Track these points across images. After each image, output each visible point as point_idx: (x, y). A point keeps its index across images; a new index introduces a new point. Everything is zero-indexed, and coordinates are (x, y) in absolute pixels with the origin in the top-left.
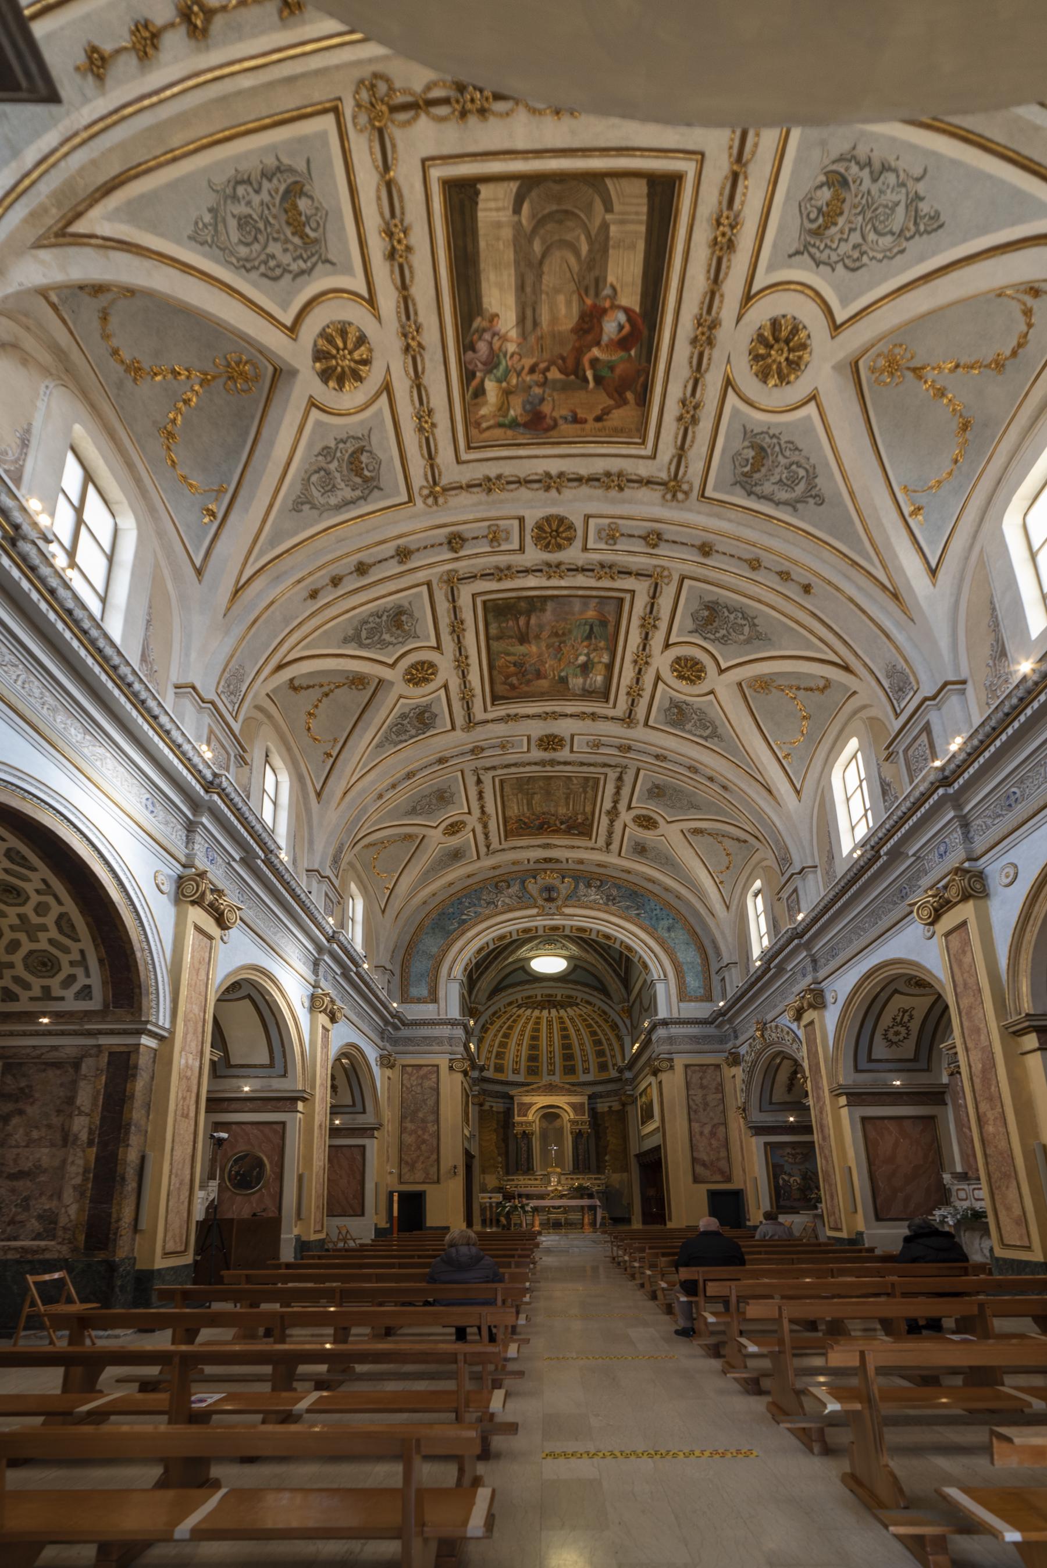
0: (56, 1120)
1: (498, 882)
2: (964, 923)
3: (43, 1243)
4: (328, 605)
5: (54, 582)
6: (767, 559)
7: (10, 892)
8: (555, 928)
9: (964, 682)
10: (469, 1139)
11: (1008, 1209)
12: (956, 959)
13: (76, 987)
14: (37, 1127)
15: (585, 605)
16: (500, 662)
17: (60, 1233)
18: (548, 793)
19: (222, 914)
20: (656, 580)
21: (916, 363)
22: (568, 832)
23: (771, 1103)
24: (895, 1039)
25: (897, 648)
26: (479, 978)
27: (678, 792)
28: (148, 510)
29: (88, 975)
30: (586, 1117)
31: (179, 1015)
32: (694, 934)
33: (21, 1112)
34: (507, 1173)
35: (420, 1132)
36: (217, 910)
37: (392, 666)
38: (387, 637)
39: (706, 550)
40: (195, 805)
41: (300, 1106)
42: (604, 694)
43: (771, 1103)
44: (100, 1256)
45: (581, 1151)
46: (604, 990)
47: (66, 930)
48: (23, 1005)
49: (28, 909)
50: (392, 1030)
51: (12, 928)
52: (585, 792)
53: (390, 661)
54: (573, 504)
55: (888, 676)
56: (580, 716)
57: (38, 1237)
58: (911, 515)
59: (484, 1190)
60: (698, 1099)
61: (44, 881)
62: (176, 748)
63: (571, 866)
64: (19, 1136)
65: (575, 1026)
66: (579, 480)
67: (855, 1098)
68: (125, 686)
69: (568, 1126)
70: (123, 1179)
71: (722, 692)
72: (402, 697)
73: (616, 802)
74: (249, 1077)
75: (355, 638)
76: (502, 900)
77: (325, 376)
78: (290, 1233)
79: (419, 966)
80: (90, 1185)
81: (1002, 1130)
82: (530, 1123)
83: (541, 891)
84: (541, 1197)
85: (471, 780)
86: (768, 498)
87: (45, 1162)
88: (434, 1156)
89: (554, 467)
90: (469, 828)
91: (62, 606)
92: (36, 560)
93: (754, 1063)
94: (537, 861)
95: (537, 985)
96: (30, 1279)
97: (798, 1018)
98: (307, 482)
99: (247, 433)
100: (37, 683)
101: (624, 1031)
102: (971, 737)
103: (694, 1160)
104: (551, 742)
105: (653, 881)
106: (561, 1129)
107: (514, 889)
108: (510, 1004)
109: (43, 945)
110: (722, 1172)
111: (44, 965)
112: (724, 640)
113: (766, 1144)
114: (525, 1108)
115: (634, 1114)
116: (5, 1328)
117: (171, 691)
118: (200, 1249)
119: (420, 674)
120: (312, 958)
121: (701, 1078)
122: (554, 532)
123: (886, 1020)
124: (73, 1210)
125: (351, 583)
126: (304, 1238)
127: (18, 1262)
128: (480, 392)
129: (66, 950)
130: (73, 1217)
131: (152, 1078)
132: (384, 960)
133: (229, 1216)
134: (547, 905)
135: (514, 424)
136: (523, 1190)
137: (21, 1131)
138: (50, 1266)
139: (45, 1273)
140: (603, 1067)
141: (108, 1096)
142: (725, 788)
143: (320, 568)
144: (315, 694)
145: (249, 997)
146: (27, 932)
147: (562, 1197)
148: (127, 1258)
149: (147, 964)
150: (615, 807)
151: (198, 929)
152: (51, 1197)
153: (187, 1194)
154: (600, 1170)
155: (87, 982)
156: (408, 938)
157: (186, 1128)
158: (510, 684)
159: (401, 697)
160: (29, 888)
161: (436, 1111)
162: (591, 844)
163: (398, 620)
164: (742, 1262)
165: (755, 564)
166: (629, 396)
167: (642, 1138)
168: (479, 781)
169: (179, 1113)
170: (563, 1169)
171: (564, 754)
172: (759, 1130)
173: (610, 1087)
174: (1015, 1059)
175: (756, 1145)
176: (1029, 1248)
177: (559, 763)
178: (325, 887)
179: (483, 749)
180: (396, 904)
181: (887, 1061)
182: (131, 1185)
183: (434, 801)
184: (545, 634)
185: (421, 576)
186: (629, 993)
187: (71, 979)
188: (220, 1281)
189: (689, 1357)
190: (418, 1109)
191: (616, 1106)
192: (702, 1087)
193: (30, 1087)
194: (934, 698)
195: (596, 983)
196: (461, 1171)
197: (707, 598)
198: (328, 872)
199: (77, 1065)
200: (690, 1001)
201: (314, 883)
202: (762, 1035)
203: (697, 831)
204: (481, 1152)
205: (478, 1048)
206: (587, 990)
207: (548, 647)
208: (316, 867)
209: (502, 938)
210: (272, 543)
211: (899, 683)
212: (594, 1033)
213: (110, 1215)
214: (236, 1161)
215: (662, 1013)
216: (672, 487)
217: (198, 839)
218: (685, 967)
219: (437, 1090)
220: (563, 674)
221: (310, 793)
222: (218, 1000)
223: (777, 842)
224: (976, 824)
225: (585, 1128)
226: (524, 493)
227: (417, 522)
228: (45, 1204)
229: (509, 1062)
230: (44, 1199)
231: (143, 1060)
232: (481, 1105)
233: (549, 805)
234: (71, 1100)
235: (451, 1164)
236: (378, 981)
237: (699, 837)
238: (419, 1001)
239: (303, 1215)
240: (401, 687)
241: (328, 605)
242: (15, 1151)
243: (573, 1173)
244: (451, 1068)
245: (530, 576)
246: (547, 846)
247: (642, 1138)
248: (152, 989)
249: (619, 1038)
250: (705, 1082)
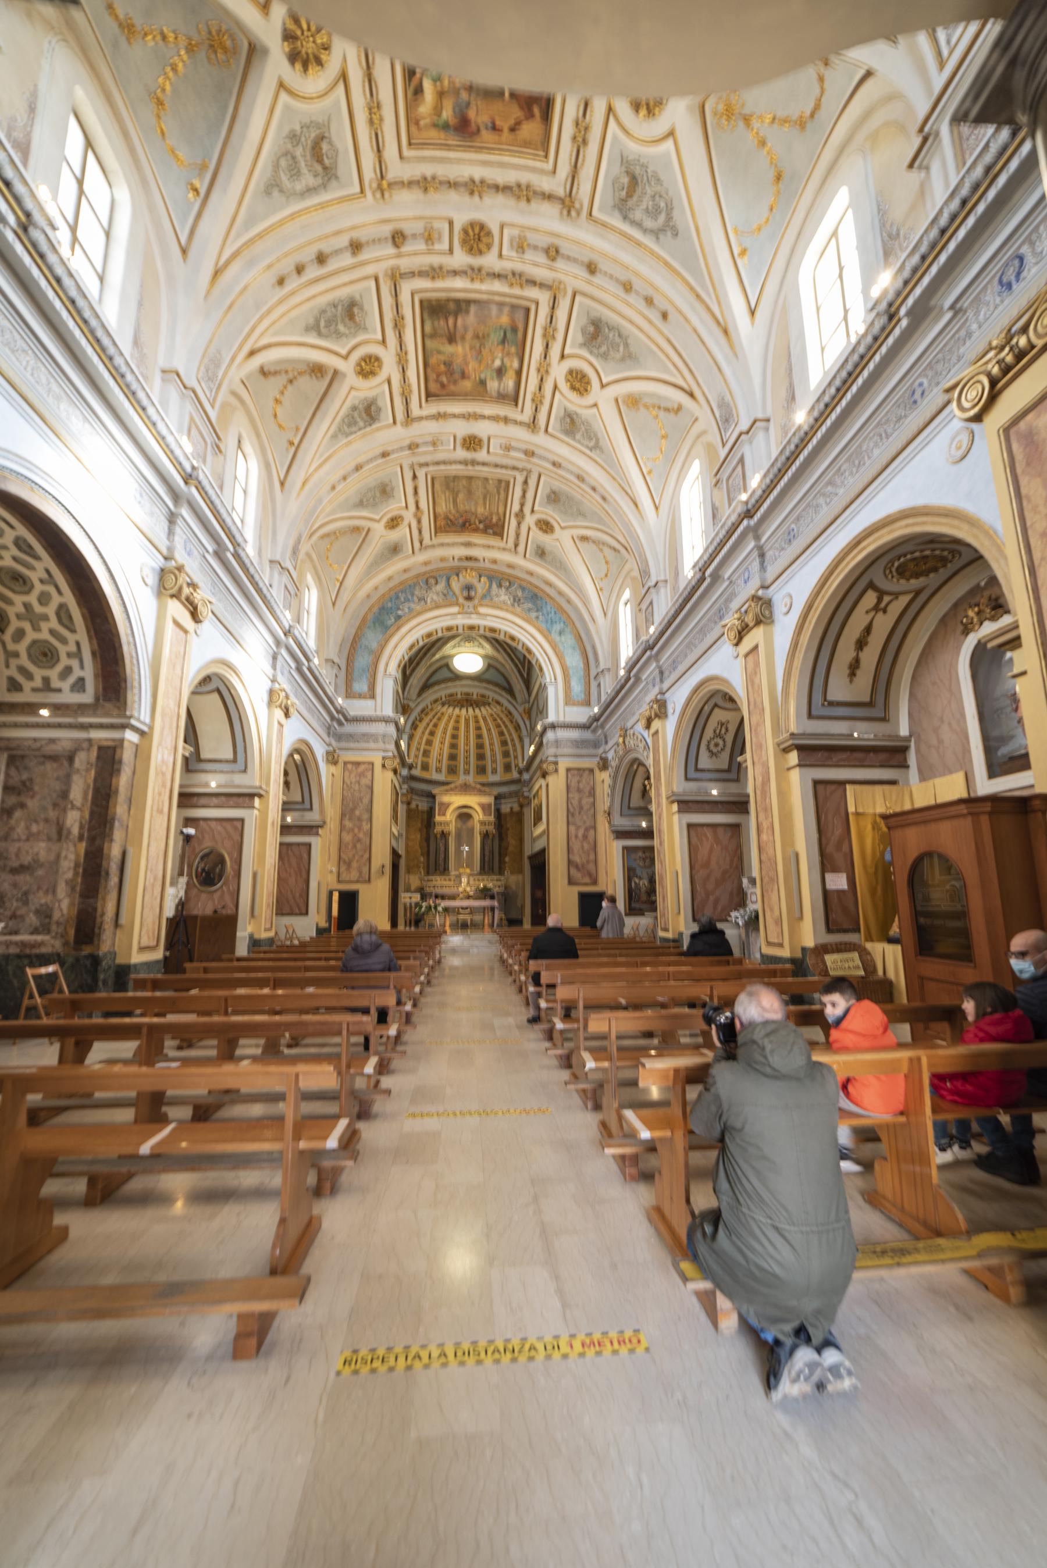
0: (52, 814)
1: (429, 579)
2: (756, 647)
3: (39, 938)
4: (293, 293)
5: (59, 271)
6: (637, 284)
7: (17, 580)
8: (472, 628)
9: (768, 420)
10: (397, 839)
11: (772, 910)
12: (751, 677)
13: (72, 679)
14: (36, 821)
15: (501, 311)
16: (433, 360)
17: (54, 927)
18: (470, 493)
19: (195, 608)
20: (554, 290)
21: (747, 111)
22: (485, 532)
23: (629, 807)
24: (715, 750)
25: (725, 381)
27: (570, 499)
28: (141, 183)
29: (82, 667)
30: (492, 818)
31: (157, 707)
32: (579, 639)
33: (22, 806)
34: (428, 873)
35: (356, 830)
36: (191, 603)
37: (346, 357)
38: (341, 328)
39: (592, 268)
40: (176, 496)
41: (257, 800)
42: (514, 399)
43: (629, 807)
44: (87, 950)
45: (487, 853)
46: (510, 691)
47: (65, 620)
48: (25, 696)
49: (32, 599)
50: (337, 723)
51: (19, 617)
52: (499, 493)
53: (344, 351)
54: (494, 212)
55: (720, 407)
56: (495, 419)
57: (35, 931)
58: (739, 255)
59: (408, 890)
60: (575, 802)
61: (48, 571)
62: (161, 439)
63: (488, 565)
64: (20, 830)
65: (487, 725)
66: (497, 188)
67: (685, 805)
68: (118, 376)
69: (477, 828)
70: (107, 874)
71: (601, 406)
72: (354, 389)
73: (522, 505)
74: (215, 772)
75: (315, 328)
76: (432, 596)
77: (293, 57)
78: (245, 930)
79: (362, 661)
80: (79, 880)
81: (771, 838)
82: (447, 824)
83: (462, 590)
84: (453, 897)
85: (408, 475)
86: (638, 225)
87: (43, 856)
88: (367, 856)
89: (478, 173)
90: (406, 522)
91: (66, 294)
92: (44, 247)
93: (618, 768)
94: (460, 559)
95: (458, 683)
96: (30, 972)
97: (648, 727)
98: (276, 166)
99: (226, 107)
100: (43, 369)
101: (524, 732)
102: (765, 476)
104: (472, 443)
105: (549, 584)
106: (471, 831)
107: (441, 586)
108: (436, 701)
109: (45, 635)
110: (590, 875)
111: (45, 655)
112: (605, 356)
113: (624, 848)
114: (445, 806)
115: (529, 815)
116: (12, 1012)
117: (158, 376)
118: (170, 945)
119: (368, 367)
120: (271, 652)
122: (476, 237)
123: (709, 733)
124: (65, 904)
125: (313, 272)
126: (256, 936)
127: (19, 956)
128: (419, 91)
129: (64, 641)
130: (65, 911)
131: (134, 773)
132: (333, 654)
133: (195, 912)
134: (467, 603)
135: (445, 127)
136: (440, 891)
137: (22, 824)
138: (45, 960)
139: (41, 965)
140: (507, 768)
141: (97, 791)
142: (604, 499)
143: (286, 255)
144: (282, 380)
145: (218, 691)
146: (31, 622)
147: (469, 897)
148: (110, 952)
149: (132, 657)
150: (521, 510)
151: (176, 623)
152: (47, 892)
153: (160, 889)
154: (501, 872)
155: (82, 674)
156: (353, 631)
157: (161, 822)
158: (442, 382)
159: (352, 388)
160: (34, 576)
161: (370, 811)
162: (502, 544)
163: (350, 311)
164: (576, 956)
165: (628, 287)
166: (536, 111)
167: (534, 840)
168: (415, 477)
169: (155, 808)
170: (472, 870)
171: (482, 455)
172: (620, 834)
173: (513, 788)
174: (783, 771)
175: (616, 848)
176: (781, 945)
177: (478, 463)
178: (285, 579)
179: (417, 446)
180: (345, 597)
181: (709, 771)
182: (114, 880)
183: (378, 494)
184: (469, 335)
185: (370, 270)
186: (530, 694)
187: (68, 670)
188: (184, 971)
189: (533, 1040)
190: (355, 809)
191: (516, 808)
192: (579, 790)
193: (31, 780)
194: (748, 432)
195: (505, 684)
196: (388, 870)
197: (593, 314)
198: (288, 564)
199: (71, 759)
200: (574, 704)
201: (276, 575)
202: (624, 742)
203: (584, 539)
204: (407, 852)
205: (409, 746)
206: (497, 689)
207: (471, 348)
208: (278, 558)
209: (429, 635)
210: (248, 225)
211: (726, 417)
212: (501, 734)
213: (95, 909)
214: (202, 858)
215: (552, 718)
216: (567, 204)
217: (178, 530)
218: (571, 672)
219: (371, 788)
220: (483, 376)
221: (279, 480)
222: (194, 693)
223: (640, 556)
224: (769, 554)
225: (491, 829)
226: (453, 196)
227: (367, 216)
228: (40, 899)
229: (433, 762)
230: (41, 894)
231: (127, 755)
232: (409, 803)
233: (471, 506)
234: (65, 794)
235: (380, 863)
236: (327, 675)
237: (585, 544)
238: (361, 696)
239: (256, 913)
240: (352, 379)
241: (293, 293)
242: (17, 845)
243: (480, 874)
244: (384, 766)
245: (458, 278)
246: (468, 545)
247: (534, 840)
248: (136, 684)
249: (521, 739)
250: (581, 786)
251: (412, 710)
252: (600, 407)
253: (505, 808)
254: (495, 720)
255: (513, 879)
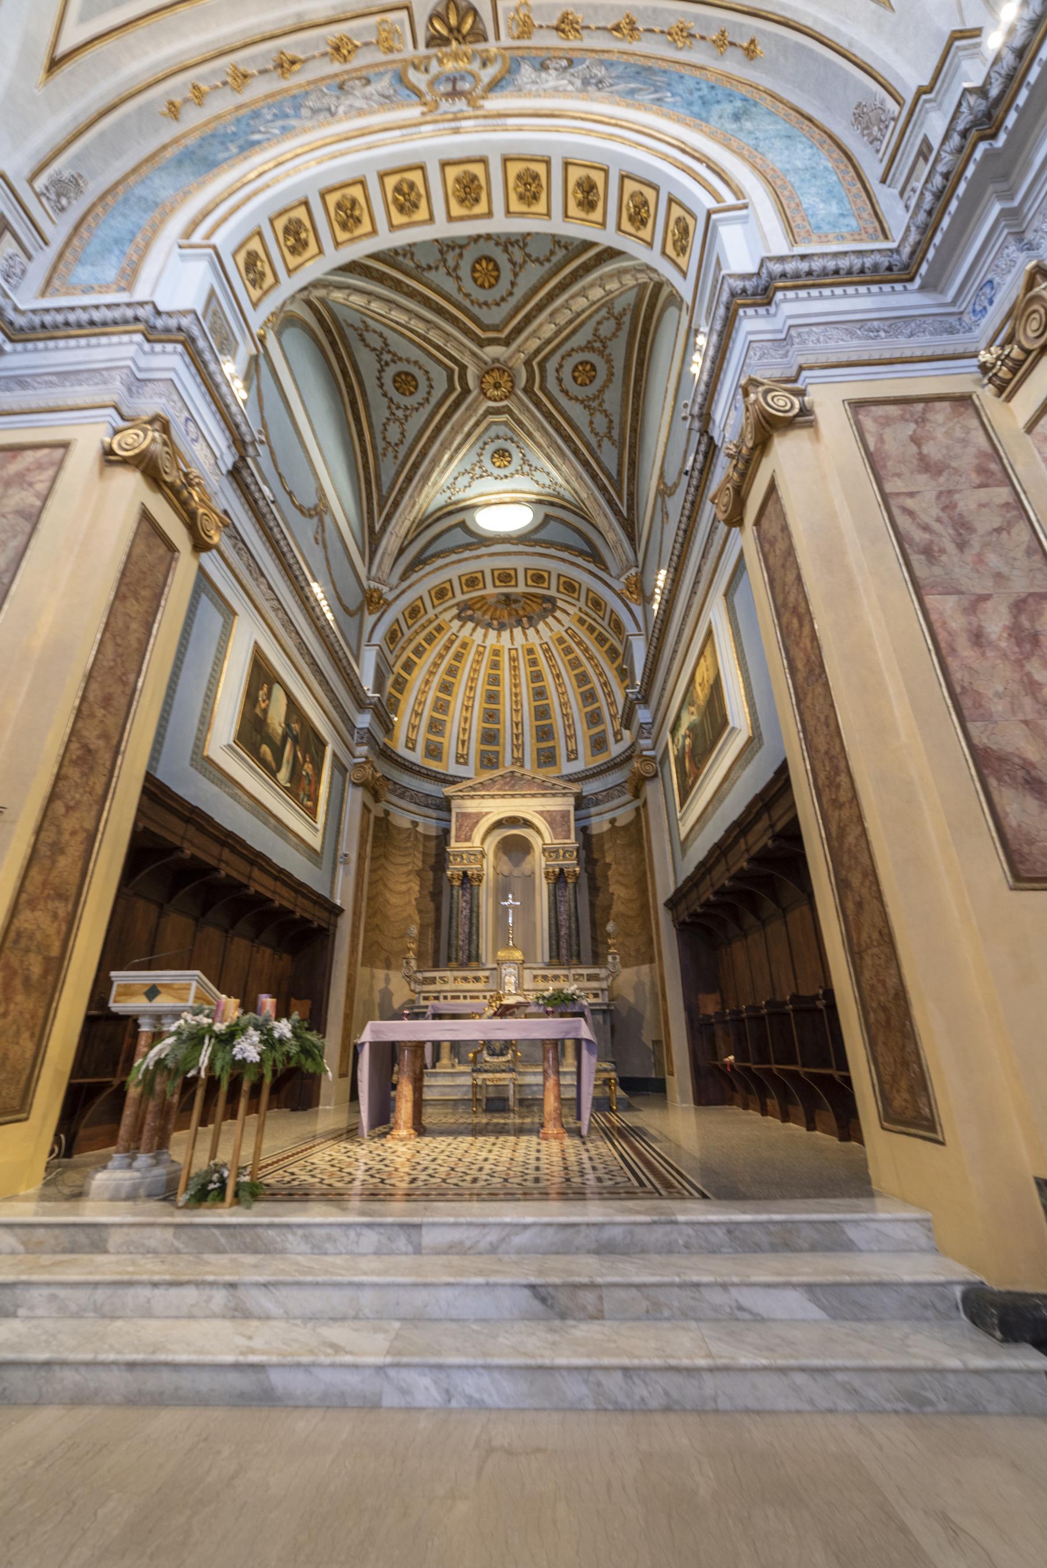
26: (384, 529)
30: (572, 841)
45: (563, 917)
60: (926, 505)
95: (483, 550)
103: (984, 760)
106: (531, 876)
121: (915, 440)
154: (597, 958)
192: (926, 465)
210: (381, 508)
225: (571, 864)
229: (450, 743)
243: (549, 965)
251: (388, 604)
252: (679, 466)
253: (599, 825)
254: (568, 651)
255: (629, 979)
